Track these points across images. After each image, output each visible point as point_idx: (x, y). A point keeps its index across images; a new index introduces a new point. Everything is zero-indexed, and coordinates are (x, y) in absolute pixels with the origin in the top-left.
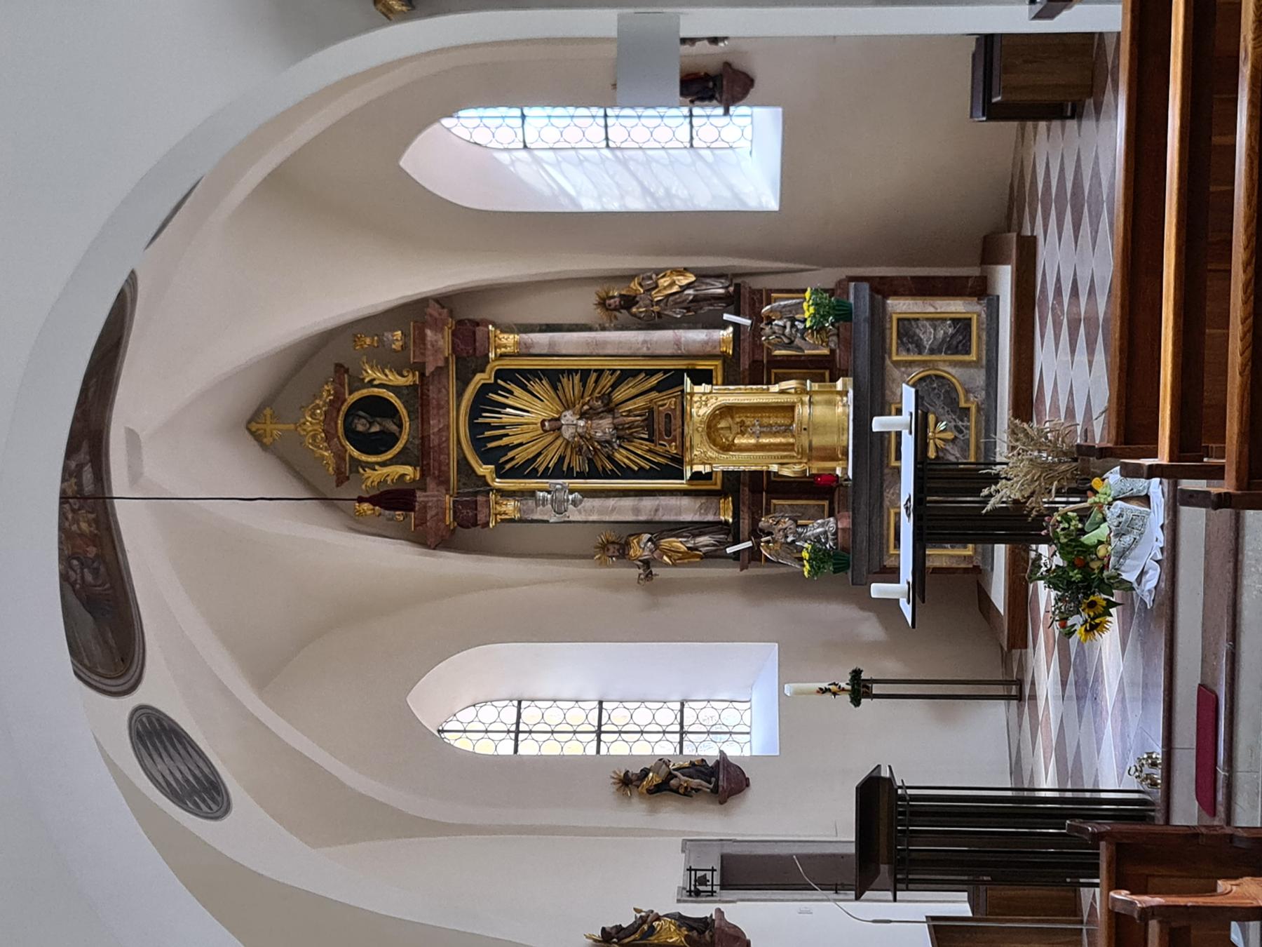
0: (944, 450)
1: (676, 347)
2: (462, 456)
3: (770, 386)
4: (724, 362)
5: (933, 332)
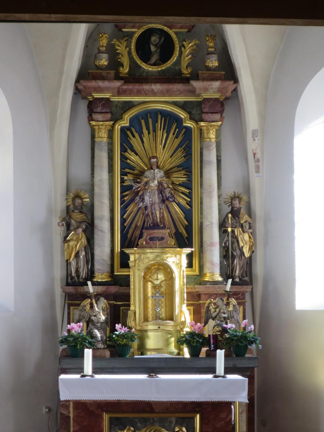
2: (135, 104)
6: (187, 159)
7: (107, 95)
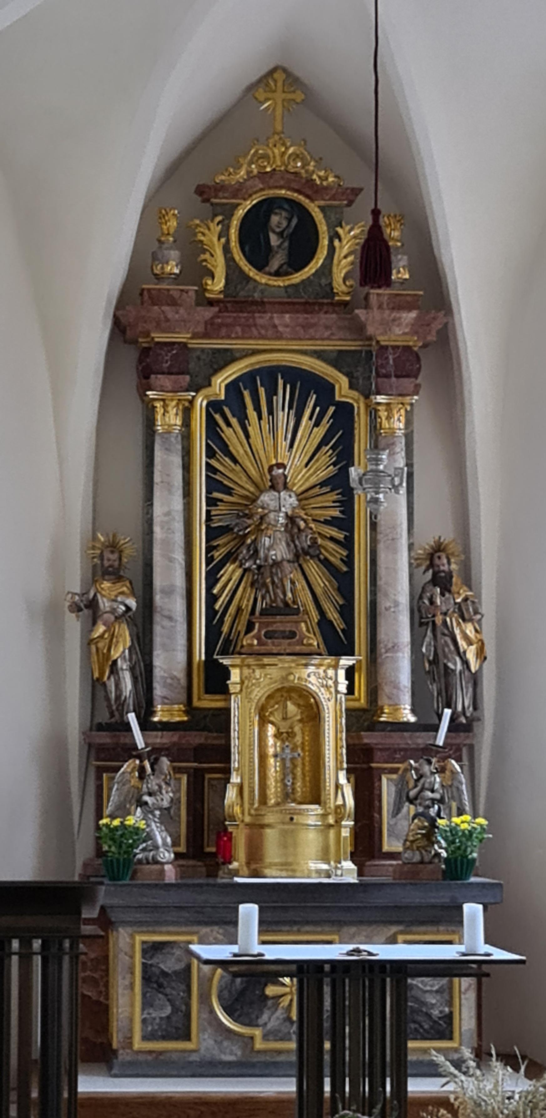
0: (276, 1006)
1: (390, 645)
2: (238, 355)
3: (345, 772)
4: (364, 710)
5: (435, 989)
6: (339, 469)
7: (182, 337)
